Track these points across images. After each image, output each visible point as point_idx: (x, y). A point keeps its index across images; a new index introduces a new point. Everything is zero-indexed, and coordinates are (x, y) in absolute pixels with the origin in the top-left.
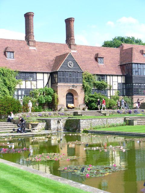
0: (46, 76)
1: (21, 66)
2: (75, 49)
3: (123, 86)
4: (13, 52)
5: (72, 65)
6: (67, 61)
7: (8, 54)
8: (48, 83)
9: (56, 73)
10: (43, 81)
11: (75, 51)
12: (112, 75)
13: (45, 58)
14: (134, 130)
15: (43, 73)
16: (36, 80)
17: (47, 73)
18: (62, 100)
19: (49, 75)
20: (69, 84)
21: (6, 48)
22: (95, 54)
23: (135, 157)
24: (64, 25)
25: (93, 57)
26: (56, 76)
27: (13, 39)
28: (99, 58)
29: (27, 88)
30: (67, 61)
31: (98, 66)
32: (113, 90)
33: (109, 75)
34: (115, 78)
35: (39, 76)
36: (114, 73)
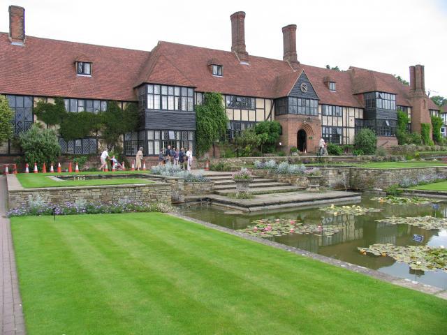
0: (268, 104)
8: (270, 114)
12: (349, 107)
16: (255, 109)
17: (270, 99)
32: (349, 128)
34: (352, 112)
35: (260, 103)
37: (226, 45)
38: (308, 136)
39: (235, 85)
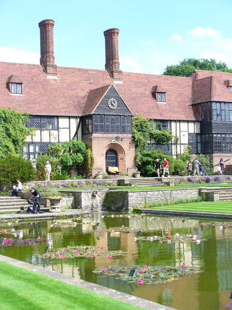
0: (74, 123)
1: (33, 106)
2: (119, 79)
3: (197, 138)
4: (21, 84)
5: (116, 105)
6: (108, 97)
7: (13, 87)
8: (76, 133)
9: (90, 117)
10: (68, 130)
11: (120, 83)
12: (180, 121)
13: (71, 93)
14: (215, 208)
15: (69, 117)
16: (58, 129)
17: (76, 117)
18: (99, 160)
19: (78, 120)
20: (110, 135)
21: (10, 78)
22: (151, 87)
23: (215, 252)
24: (103, 39)
25: (148, 92)
26: (90, 122)
27: (22, 62)
28: (158, 93)
29: (43, 141)
30: (108, 97)
31: (158, 106)
32: (181, 144)
33: (175, 121)
34: (184, 126)
35: (63, 122)
36: (183, 118)
37: (40, 141)
38: (120, 156)
39: (35, 103)
